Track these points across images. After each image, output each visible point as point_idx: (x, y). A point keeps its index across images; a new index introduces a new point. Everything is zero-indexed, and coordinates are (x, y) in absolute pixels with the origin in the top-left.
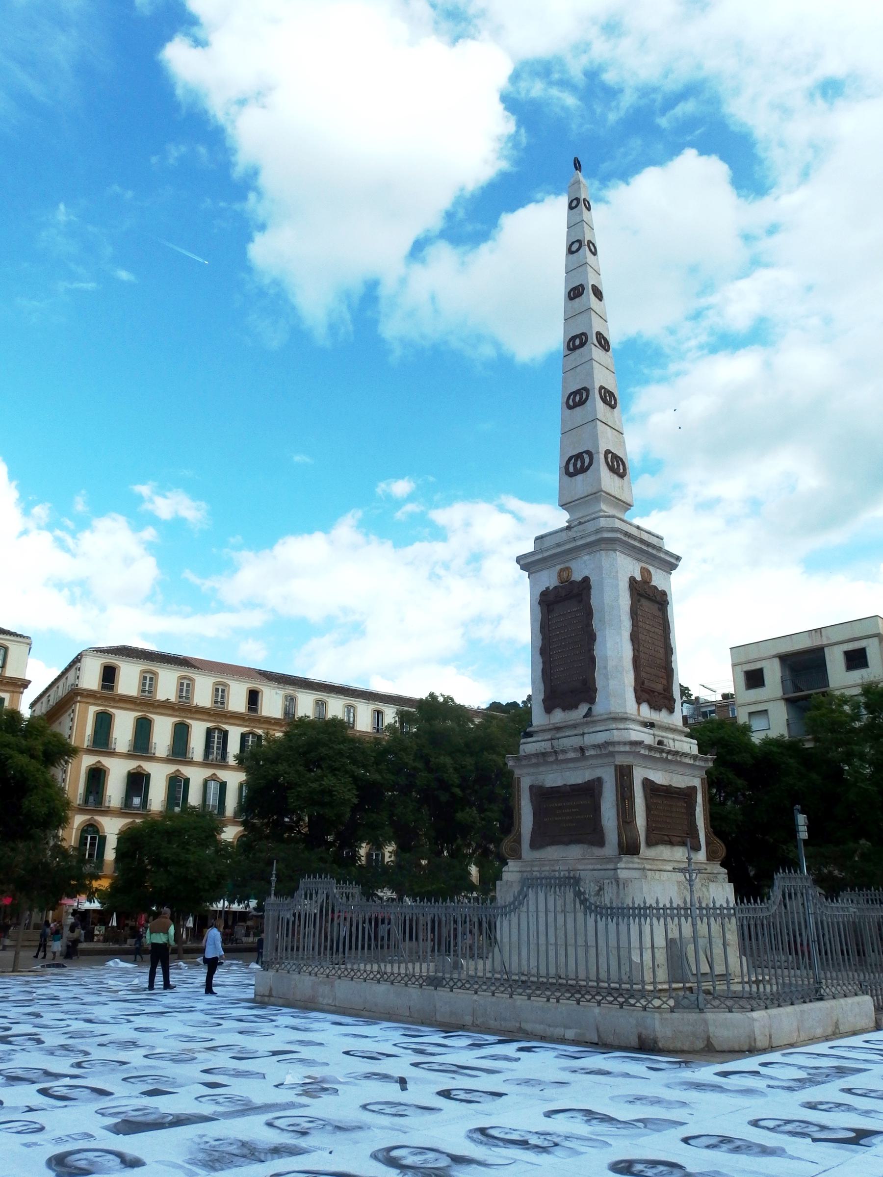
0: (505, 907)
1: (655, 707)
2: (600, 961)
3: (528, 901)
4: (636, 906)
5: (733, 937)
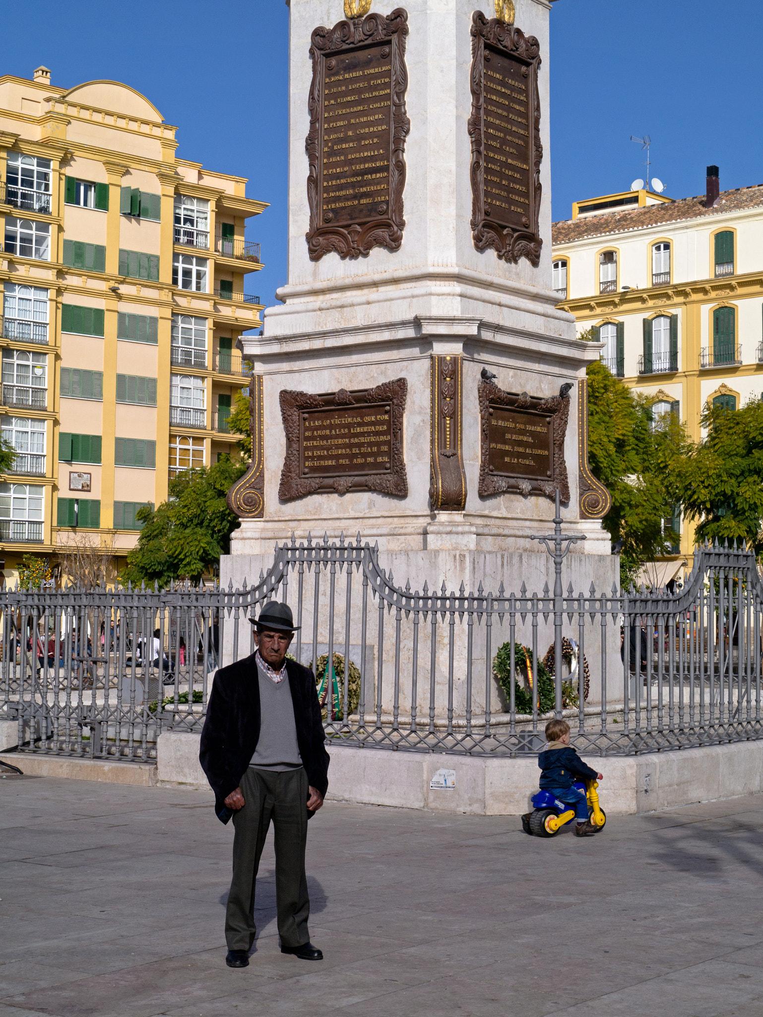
0: (244, 594)
2: (428, 687)
3: (285, 585)
5: (615, 641)
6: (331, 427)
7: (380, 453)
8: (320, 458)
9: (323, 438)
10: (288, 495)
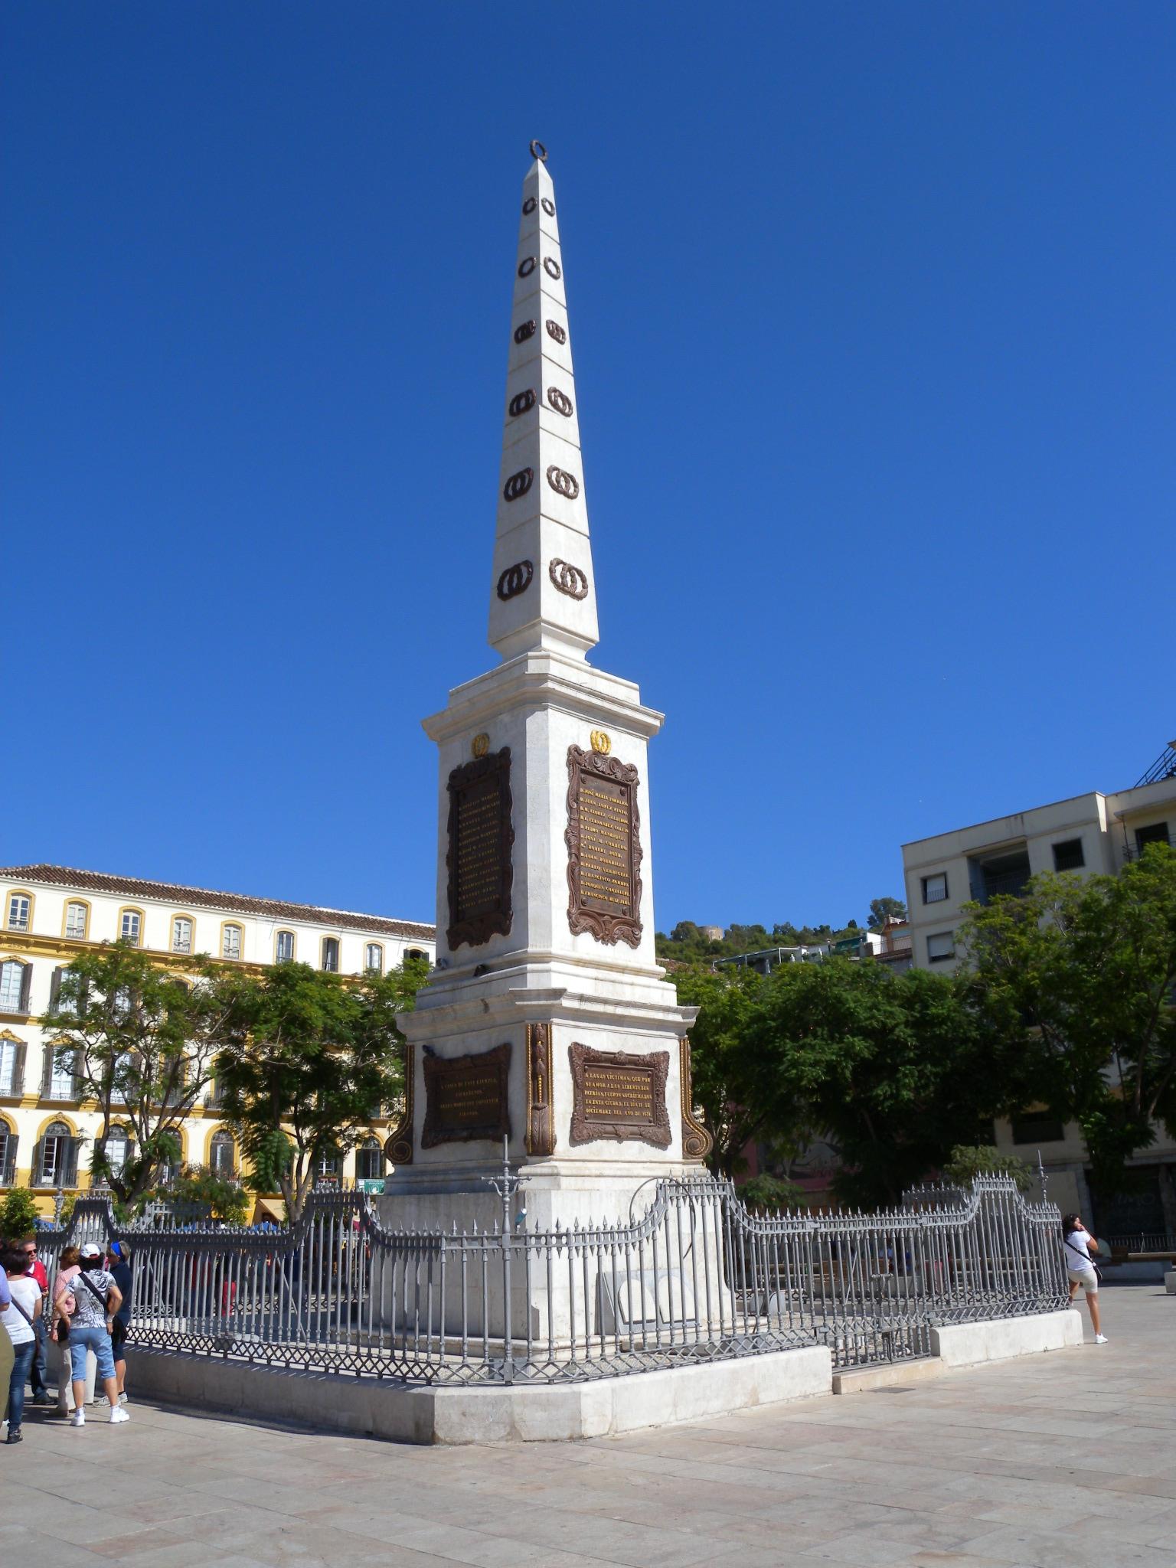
1: (606, 937)
4: (542, 1231)
6: (606, 1080)
7: (644, 1108)
8: (598, 1106)
9: (599, 1089)
10: (575, 1140)
